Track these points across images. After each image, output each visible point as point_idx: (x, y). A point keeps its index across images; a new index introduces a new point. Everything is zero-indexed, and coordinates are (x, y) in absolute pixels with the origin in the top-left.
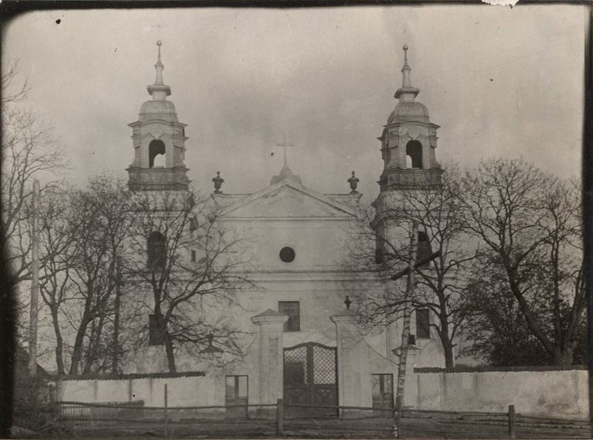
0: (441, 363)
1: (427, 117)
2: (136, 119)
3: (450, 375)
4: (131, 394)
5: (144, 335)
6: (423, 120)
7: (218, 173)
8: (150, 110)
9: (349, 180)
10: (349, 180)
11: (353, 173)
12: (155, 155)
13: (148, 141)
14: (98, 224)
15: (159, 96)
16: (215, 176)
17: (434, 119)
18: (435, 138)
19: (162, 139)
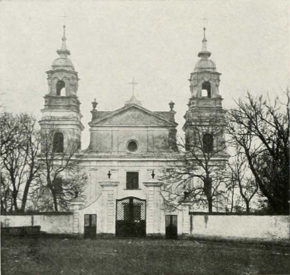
0: (206, 210)
1: (214, 68)
2: (50, 69)
3: (210, 217)
4: (32, 222)
5: (252, 267)
6: (211, 70)
7: (95, 99)
8: (57, 63)
9: (93, 103)
10: (93, 103)
11: (95, 99)
12: (61, 89)
13: (56, 81)
14: (193, 150)
15: (63, 56)
16: (93, 101)
17: (218, 71)
18: (219, 81)
19: (64, 80)
